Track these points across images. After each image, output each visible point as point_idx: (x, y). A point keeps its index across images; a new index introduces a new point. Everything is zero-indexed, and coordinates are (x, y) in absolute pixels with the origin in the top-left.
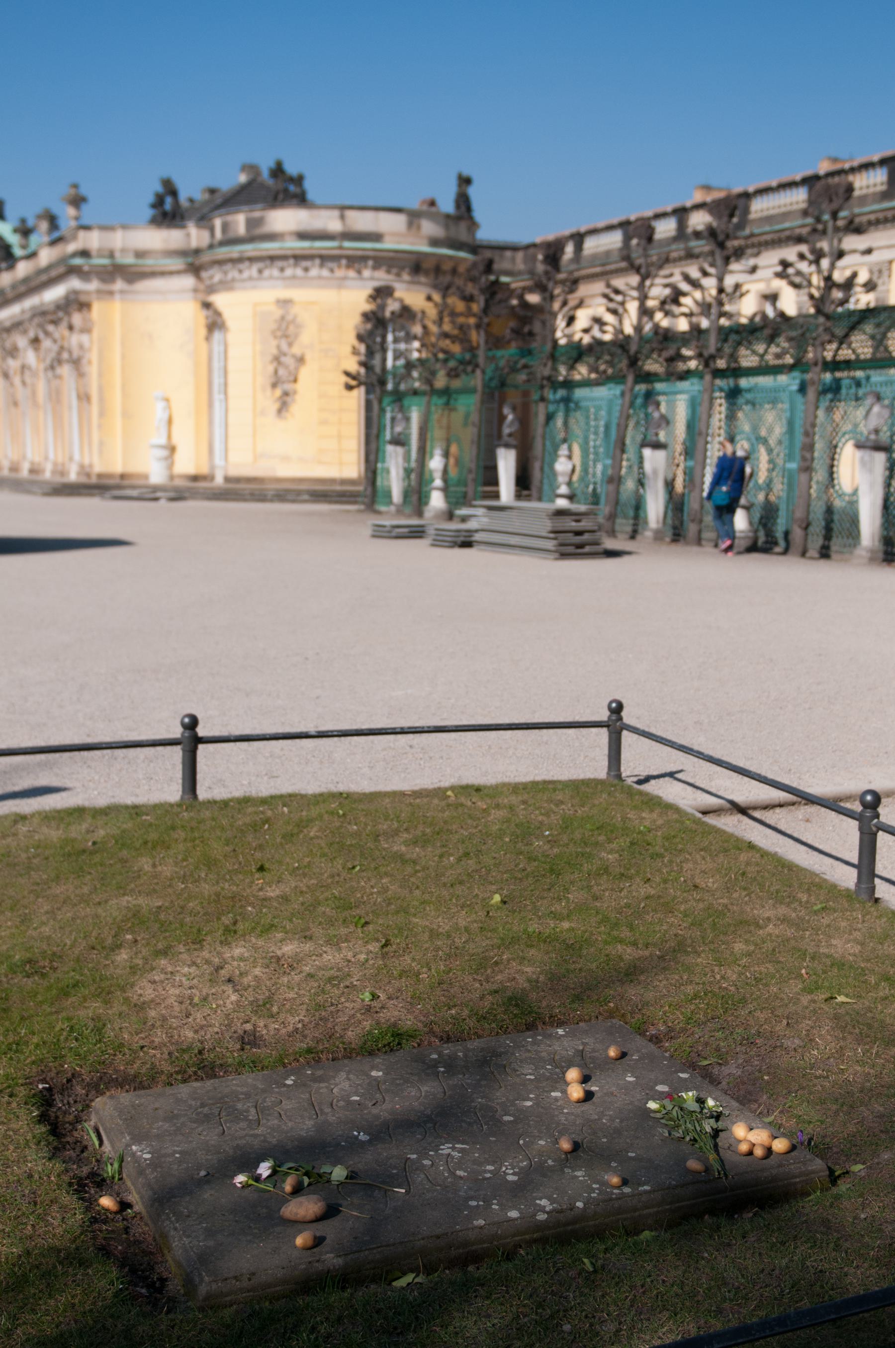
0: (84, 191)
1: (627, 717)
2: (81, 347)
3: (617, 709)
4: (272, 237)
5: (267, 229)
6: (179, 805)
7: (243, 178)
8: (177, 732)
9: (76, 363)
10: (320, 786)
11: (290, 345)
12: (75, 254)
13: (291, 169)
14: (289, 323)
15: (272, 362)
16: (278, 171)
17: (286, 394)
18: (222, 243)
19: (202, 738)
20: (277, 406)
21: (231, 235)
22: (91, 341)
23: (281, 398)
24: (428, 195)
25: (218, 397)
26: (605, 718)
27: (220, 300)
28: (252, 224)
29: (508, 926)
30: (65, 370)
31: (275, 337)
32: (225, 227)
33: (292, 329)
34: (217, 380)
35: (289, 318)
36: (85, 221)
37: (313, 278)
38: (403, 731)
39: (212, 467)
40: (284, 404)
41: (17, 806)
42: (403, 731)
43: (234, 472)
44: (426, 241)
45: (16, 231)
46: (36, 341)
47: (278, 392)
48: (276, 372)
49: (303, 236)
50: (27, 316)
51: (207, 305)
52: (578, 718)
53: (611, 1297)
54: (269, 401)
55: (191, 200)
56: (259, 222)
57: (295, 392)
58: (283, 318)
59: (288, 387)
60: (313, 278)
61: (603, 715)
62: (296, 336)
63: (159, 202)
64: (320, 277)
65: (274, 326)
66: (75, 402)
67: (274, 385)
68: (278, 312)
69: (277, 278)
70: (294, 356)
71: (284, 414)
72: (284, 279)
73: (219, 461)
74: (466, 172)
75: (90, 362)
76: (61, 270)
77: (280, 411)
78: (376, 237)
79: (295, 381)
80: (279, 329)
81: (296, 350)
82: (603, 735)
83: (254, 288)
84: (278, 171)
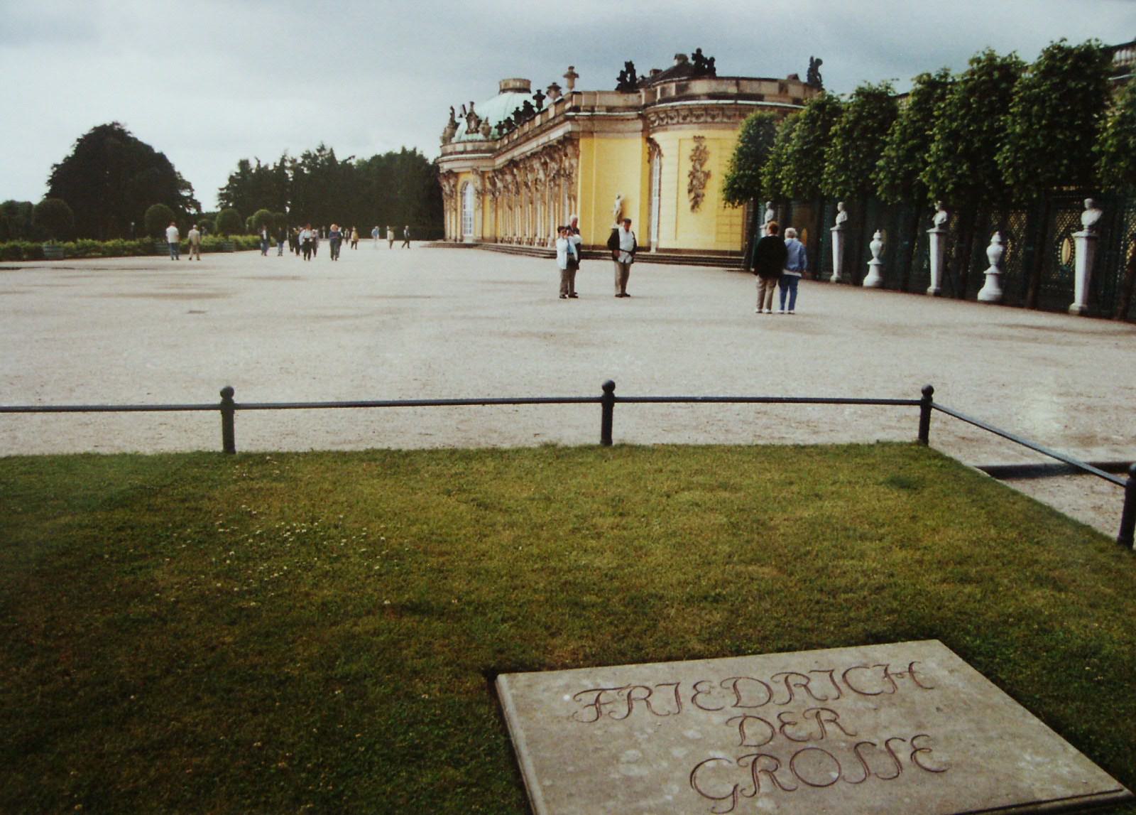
0: (576, 71)
1: (936, 398)
2: (571, 166)
3: (928, 392)
4: (692, 97)
5: (689, 92)
6: (598, 446)
7: (675, 63)
8: (218, 400)
9: (569, 176)
10: (856, 436)
11: (702, 165)
12: (570, 110)
13: (706, 54)
14: (701, 151)
15: (689, 176)
16: (698, 56)
17: (697, 196)
18: (660, 102)
19: (237, 404)
20: (691, 204)
21: (667, 96)
22: (578, 163)
23: (694, 198)
24: (792, 72)
25: (655, 199)
26: (919, 399)
27: (658, 137)
28: (680, 89)
29: (672, 517)
30: (562, 181)
31: (692, 160)
32: (663, 91)
33: (703, 155)
34: (655, 187)
35: (702, 148)
36: (576, 89)
37: (717, 123)
38: (484, 402)
39: (650, 243)
40: (696, 203)
41: (1077, 454)
42: (484, 402)
43: (663, 245)
44: (791, 101)
45: (534, 98)
46: (545, 164)
47: (693, 195)
48: (692, 181)
49: (711, 96)
50: (540, 148)
51: (650, 141)
52: (770, 395)
53: (264, 718)
54: (686, 201)
55: (643, 77)
56: (686, 87)
57: (703, 195)
58: (697, 148)
59: (700, 191)
60: (717, 123)
61: (599, 393)
62: (705, 160)
63: (622, 77)
64: (722, 122)
65: (692, 153)
66: (567, 202)
67: (690, 191)
68: (694, 145)
69: (695, 123)
70: (703, 172)
71: (696, 209)
72: (698, 123)
73: (654, 239)
74: (572, 65)
75: (577, 175)
76: (561, 118)
77: (693, 207)
78: (760, 97)
79: (704, 187)
80: (694, 155)
81: (706, 168)
82: (598, 407)
83: (680, 129)
84: (698, 56)
